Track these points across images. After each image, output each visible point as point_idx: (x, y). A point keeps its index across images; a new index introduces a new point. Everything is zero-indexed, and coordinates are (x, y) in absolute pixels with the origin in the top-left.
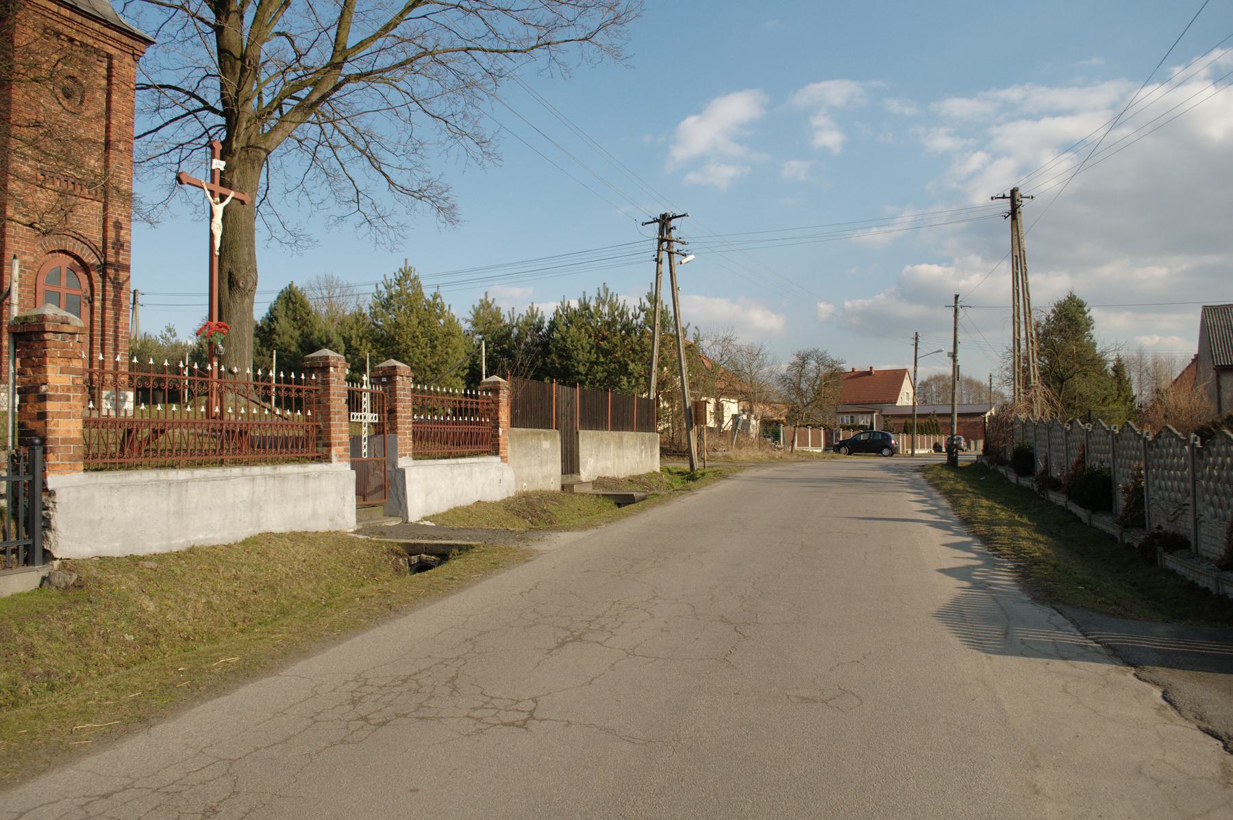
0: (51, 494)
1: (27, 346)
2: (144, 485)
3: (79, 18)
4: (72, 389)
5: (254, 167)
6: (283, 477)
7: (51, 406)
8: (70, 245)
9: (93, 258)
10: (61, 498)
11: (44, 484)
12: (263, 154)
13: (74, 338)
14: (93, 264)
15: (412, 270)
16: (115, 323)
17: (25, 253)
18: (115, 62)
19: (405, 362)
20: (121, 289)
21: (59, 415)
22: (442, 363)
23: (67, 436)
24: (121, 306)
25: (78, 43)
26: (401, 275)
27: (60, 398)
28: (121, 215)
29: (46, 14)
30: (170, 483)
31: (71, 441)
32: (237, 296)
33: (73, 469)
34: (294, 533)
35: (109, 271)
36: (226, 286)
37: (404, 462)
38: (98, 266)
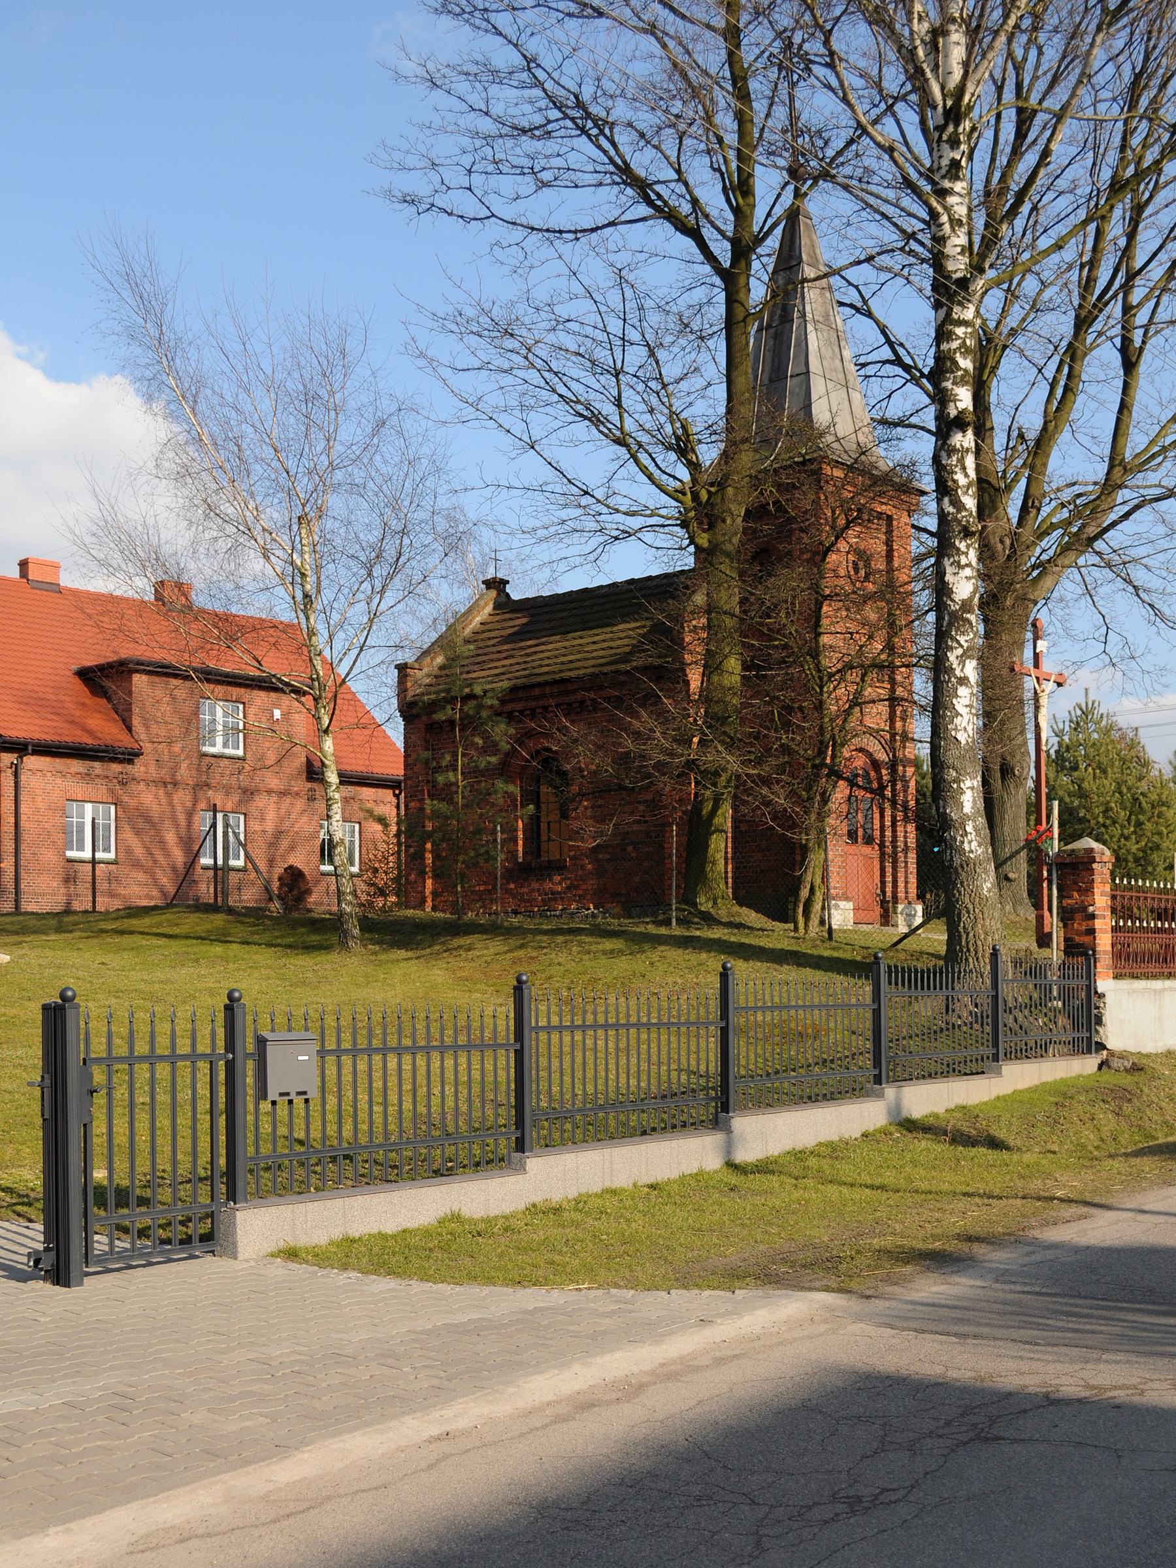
0: (1101, 996)
1: (1073, 874)
10: (1109, 999)
11: (1095, 989)
15: (1096, 705)
19: (1104, 843)
22: (1151, 849)
26: (1079, 713)
32: (1012, 786)
37: (1104, 984)
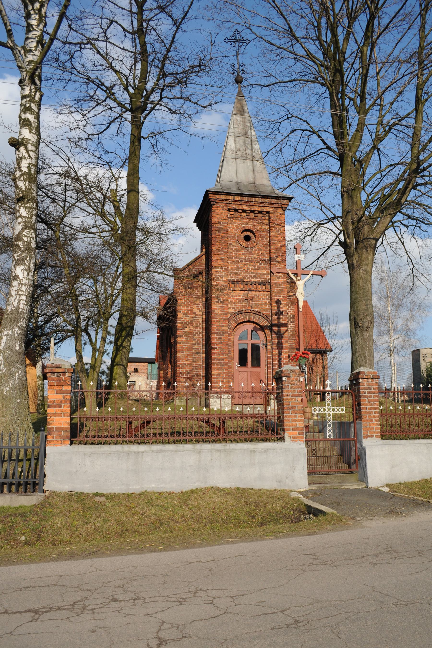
2: (171, 451)
3: (245, 199)
4: (63, 401)
5: (367, 251)
6: (230, 451)
7: (50, 411)
8: (251, 317)
9: (265, 323)
12: (373, 242)
13: (65, 375)
14: (266, 326)
16: (279, 356)
17: (223, 326)
18: (272, 215)
20: (282, 337)
21: (55, 415)
23: (60, 426)
24: (282, 347)
25: (241, 211)
27: (55, 406)
28: (280, 296)
29: (228, 202)
30: (129, 453)
31: (62, 429)
33: (62, 443)
34: (239, 489)
35: (273, 328)
36: (353, 327)
38: (269, 326)
